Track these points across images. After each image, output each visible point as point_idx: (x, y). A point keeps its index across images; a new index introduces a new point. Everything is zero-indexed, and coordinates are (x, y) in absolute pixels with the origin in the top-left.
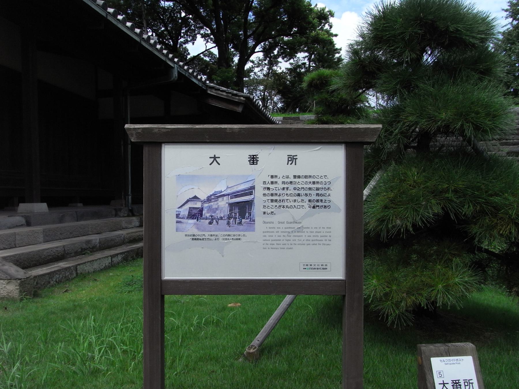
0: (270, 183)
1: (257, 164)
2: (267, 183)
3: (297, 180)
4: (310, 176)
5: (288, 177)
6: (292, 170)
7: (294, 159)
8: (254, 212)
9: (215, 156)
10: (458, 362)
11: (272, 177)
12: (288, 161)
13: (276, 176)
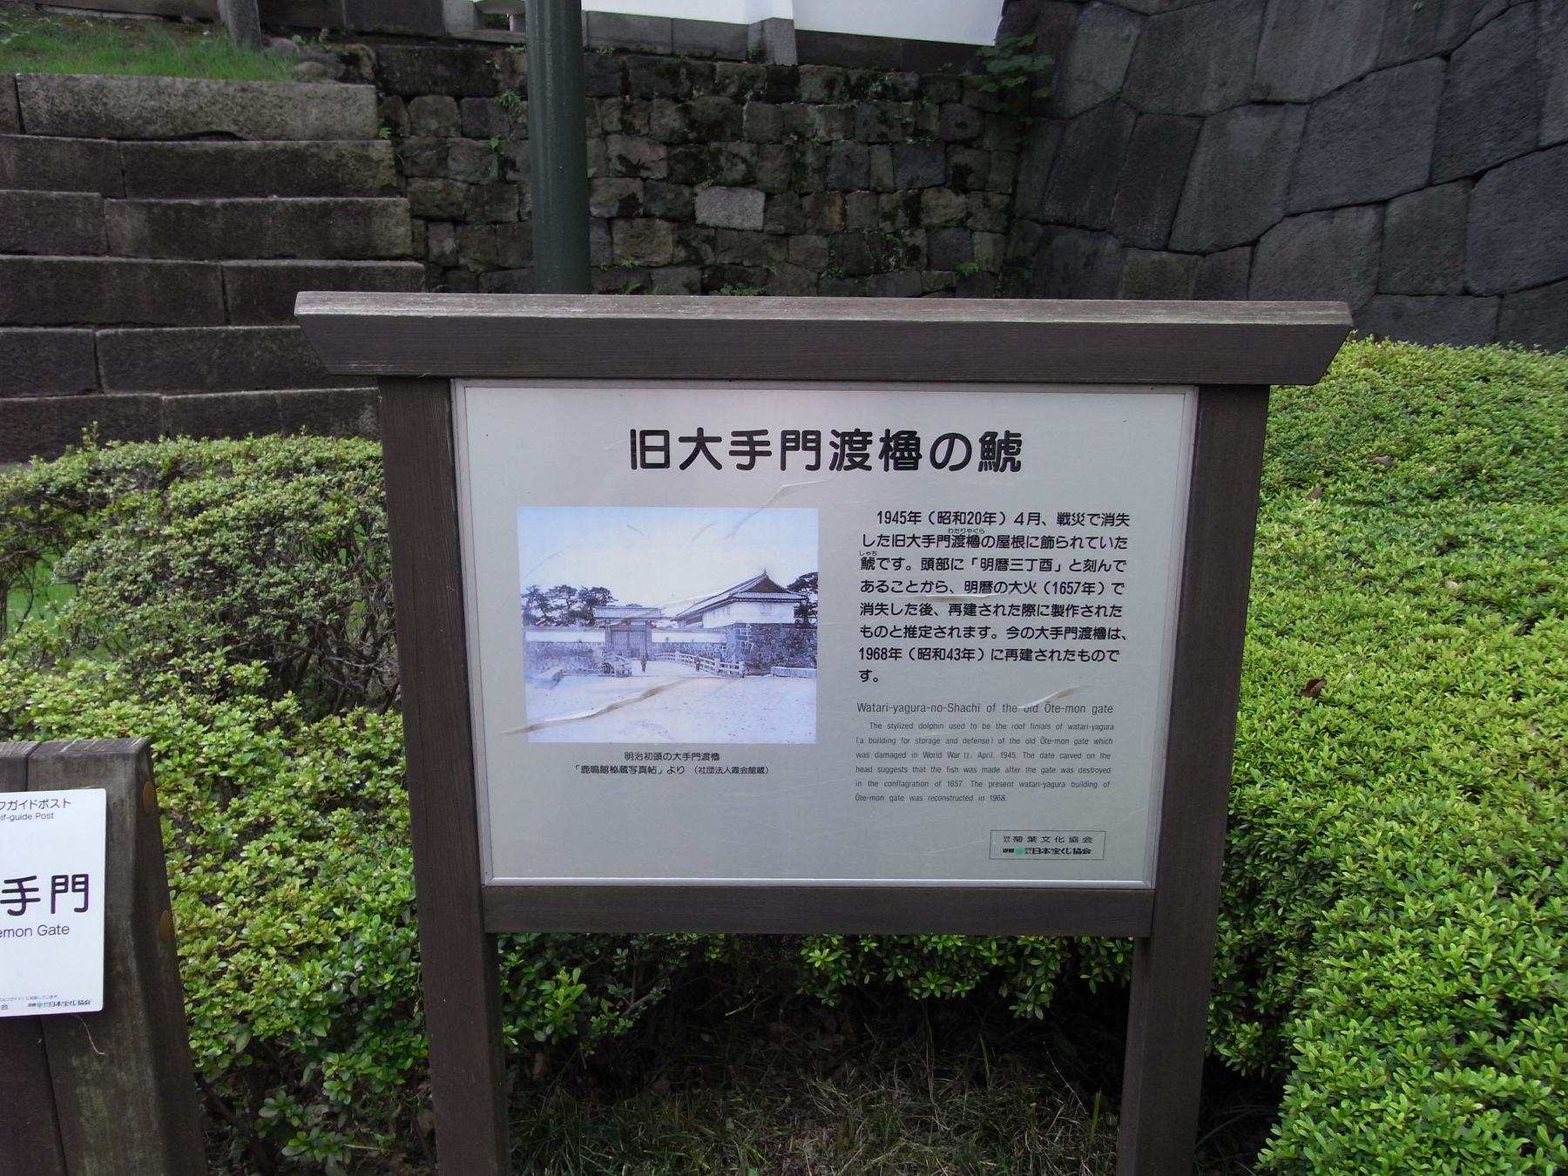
3: (1068, 532)
8: (714, 621)
9: (700, 430)
10: (46, 811)
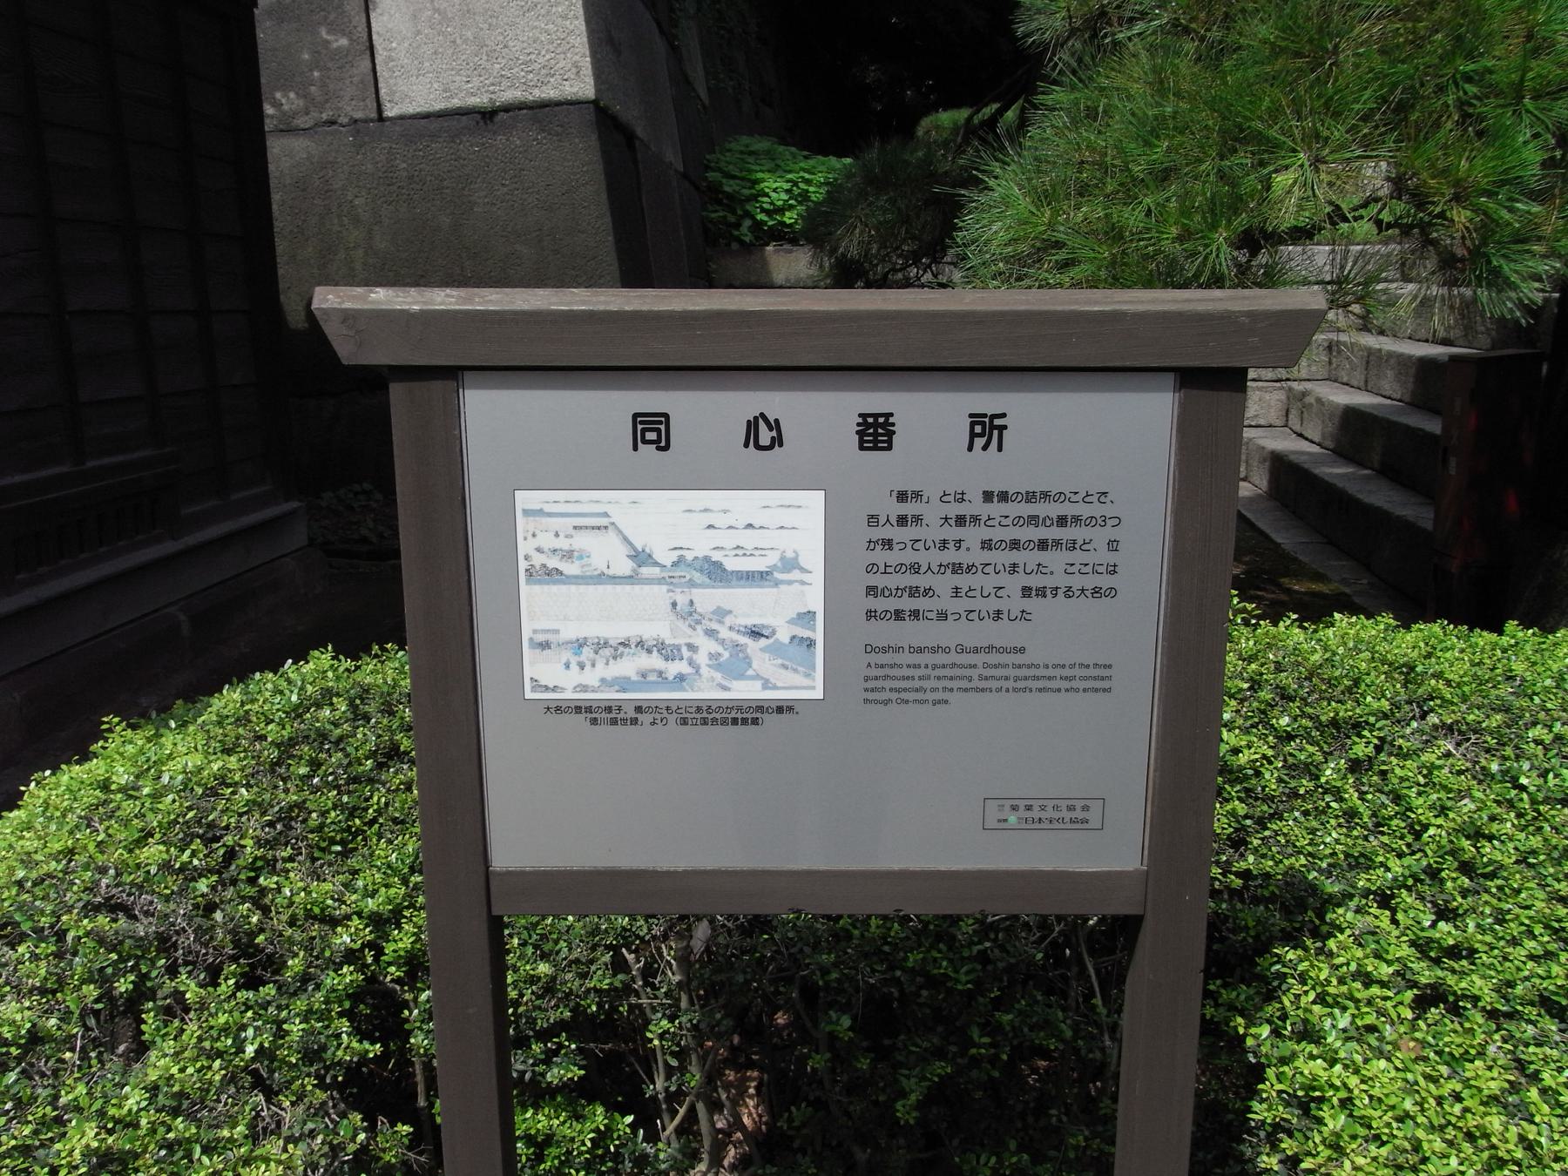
0: (893, 520)
1: (890, 448)
2: (883, 520)
3: (996, 509)
4: (1045, 495)
5: (961, 498)
6: (990, 469)
7: (993, 427)
11: (902, 497)
12: (973, 435)
13: (917, 495)
